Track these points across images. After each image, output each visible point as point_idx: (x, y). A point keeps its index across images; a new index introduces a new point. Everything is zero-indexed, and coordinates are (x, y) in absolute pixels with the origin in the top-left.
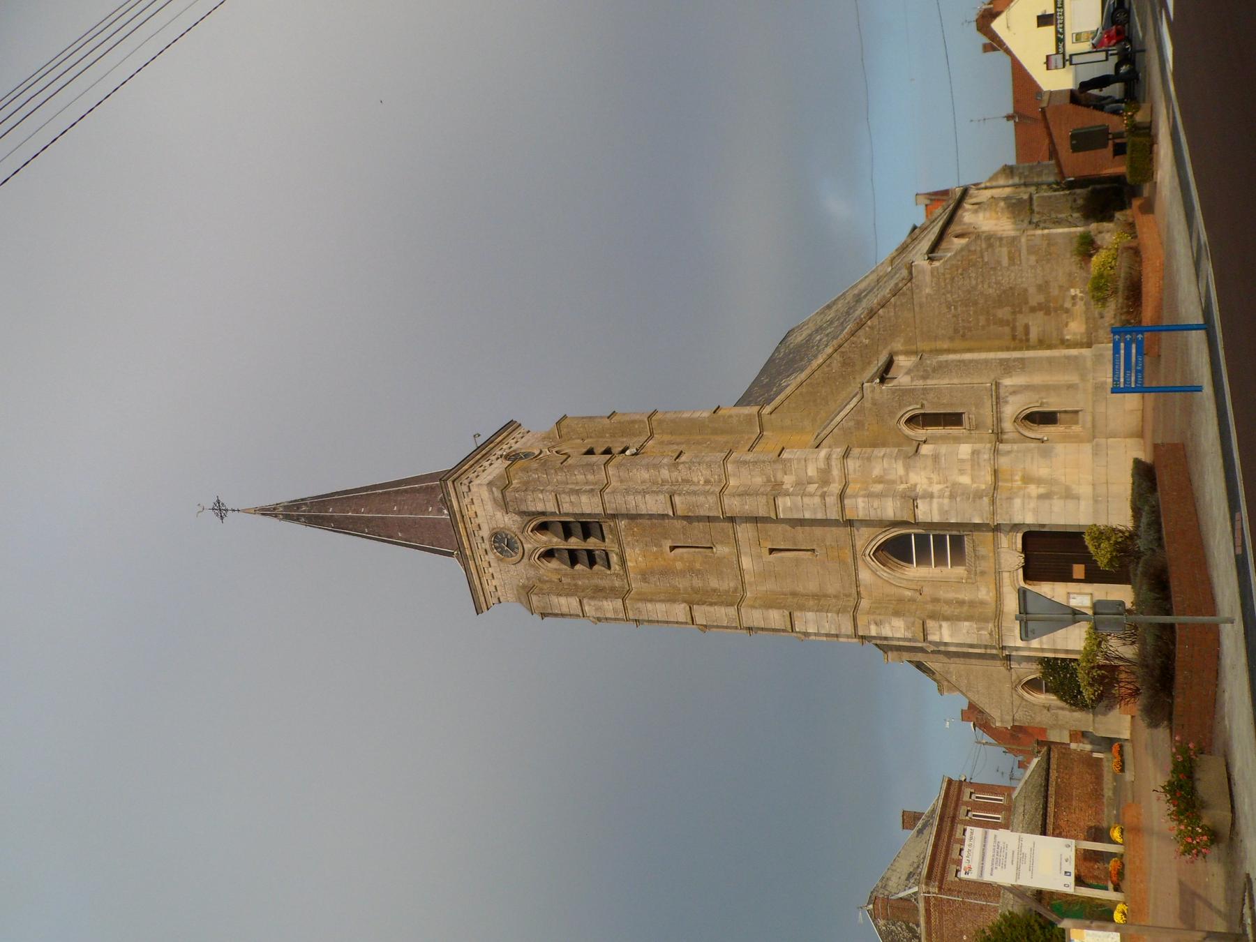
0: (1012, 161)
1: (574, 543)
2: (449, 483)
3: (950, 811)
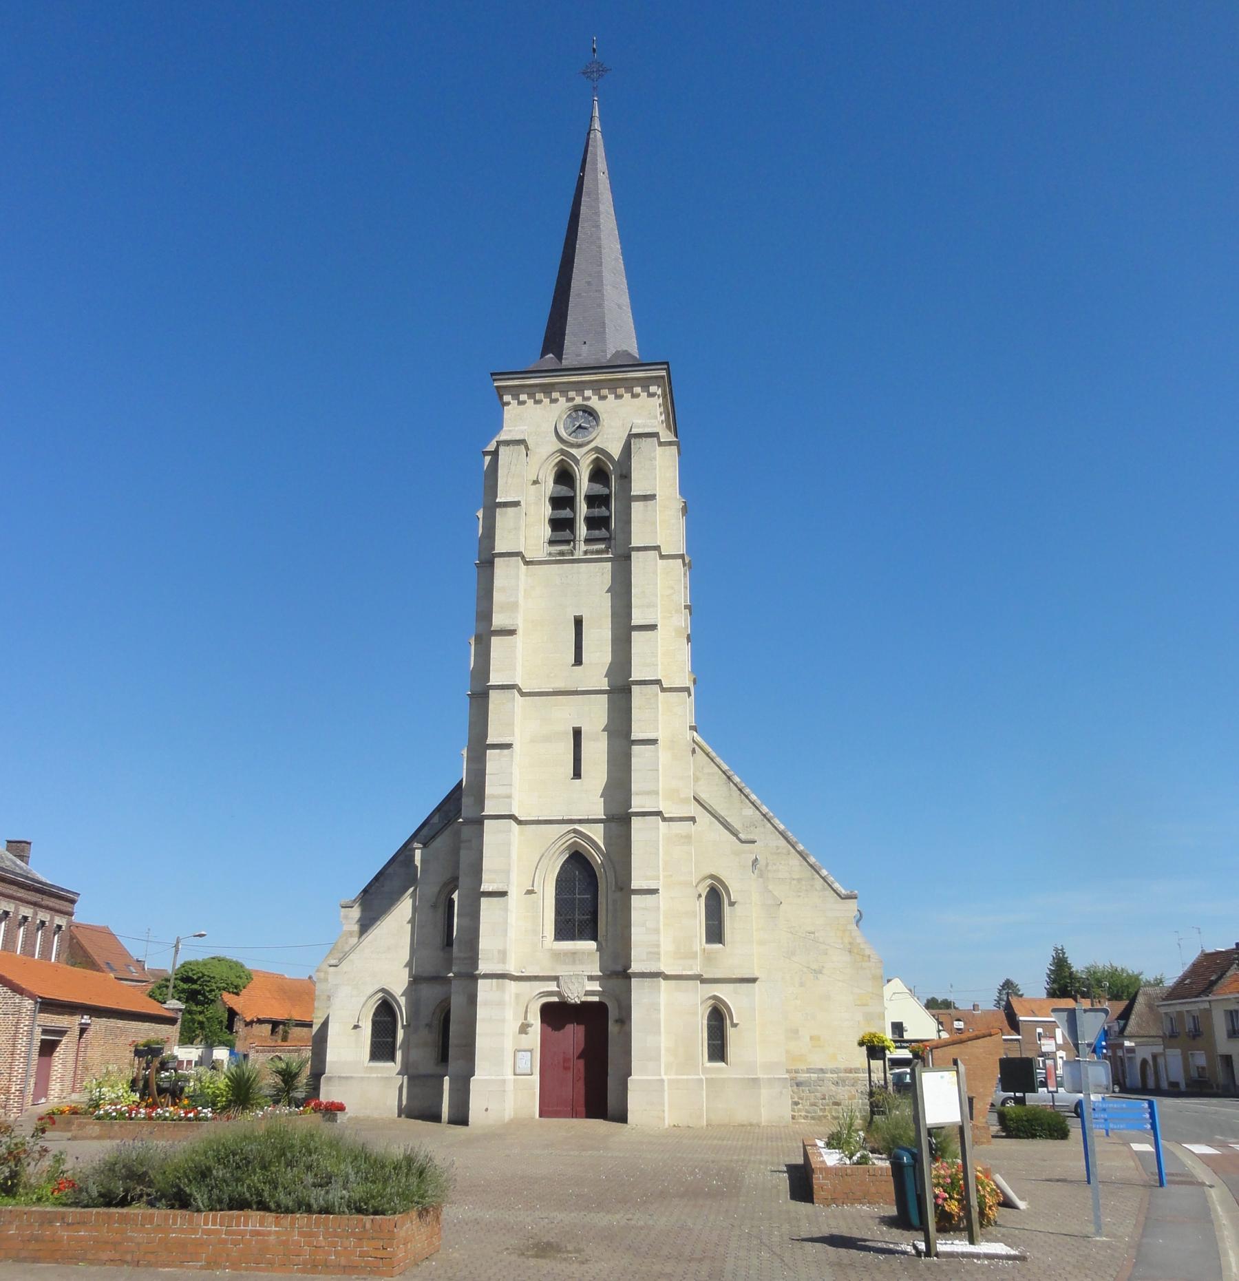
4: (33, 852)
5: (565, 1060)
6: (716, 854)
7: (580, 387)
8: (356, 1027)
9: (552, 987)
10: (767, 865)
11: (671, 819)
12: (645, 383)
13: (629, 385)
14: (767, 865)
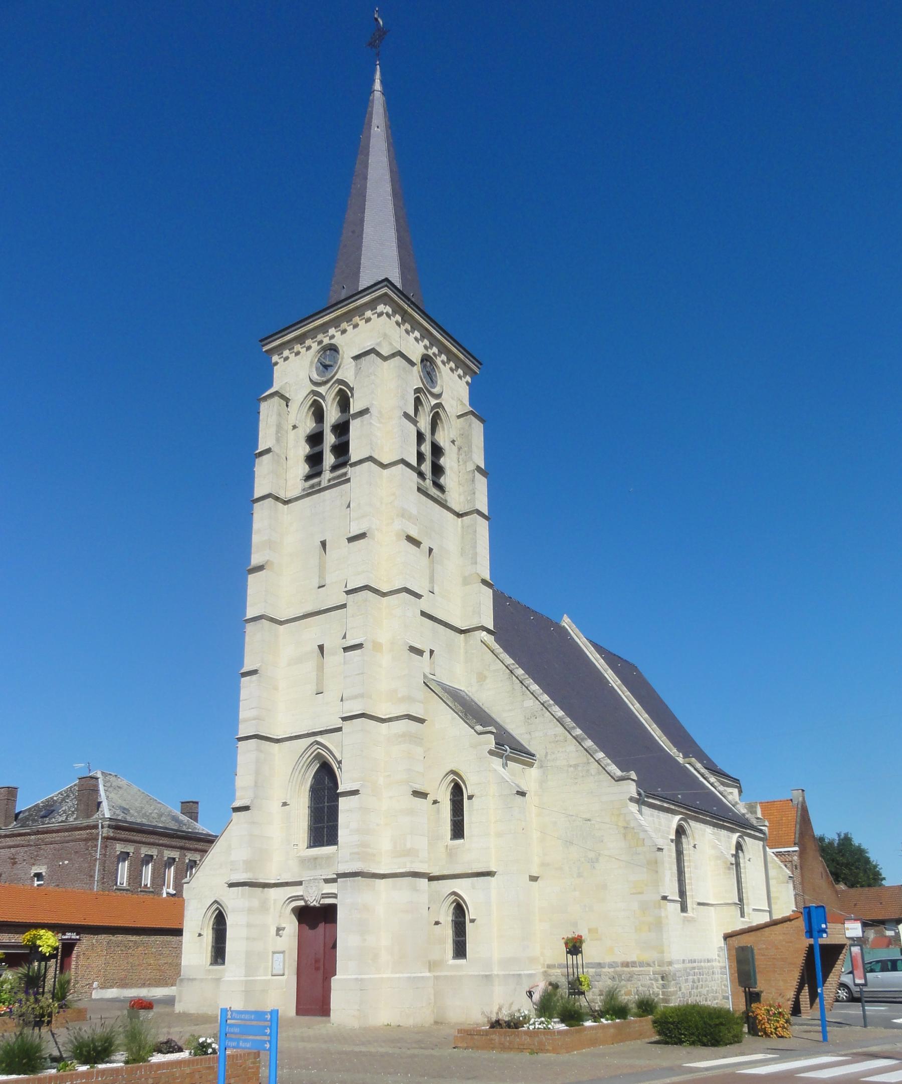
1: (330, 439)
3: (188, 844)
4: (202, 810)
5: (317, 961)
6: (458, 747)
7: (324, 328)
8: (200, 935)
10: (546, 756)
11: (390, 720)
12: (372, 305)
14: (546, 756)
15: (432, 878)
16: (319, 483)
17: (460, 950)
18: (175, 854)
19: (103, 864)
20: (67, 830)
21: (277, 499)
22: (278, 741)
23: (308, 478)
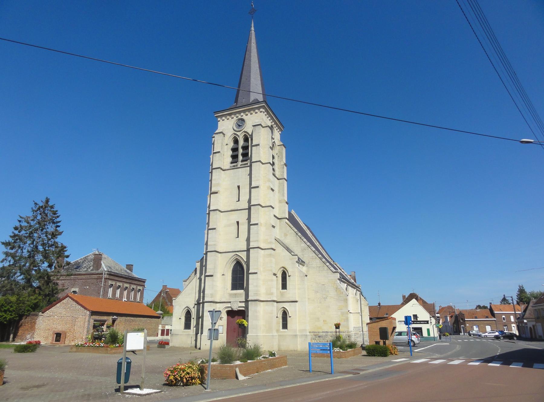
0: (381, 304)
1: (241, 151)
2: (264, 104)
3: (134, 282)
4: (134, 268)
5: (234, 329)
6: (285, 260)
7: (239, 112)
9: (229, 305)
11: (265, 249)
12: (258, 108)
13: (253, 109)
15: (277, 302)
16: (237, 166)
17: (285, 326)
18: (128, 285)
19: (104, 288)
20: (88, 275)
21: (221, 169)
22: (220, 253)
23: (232, 163)
